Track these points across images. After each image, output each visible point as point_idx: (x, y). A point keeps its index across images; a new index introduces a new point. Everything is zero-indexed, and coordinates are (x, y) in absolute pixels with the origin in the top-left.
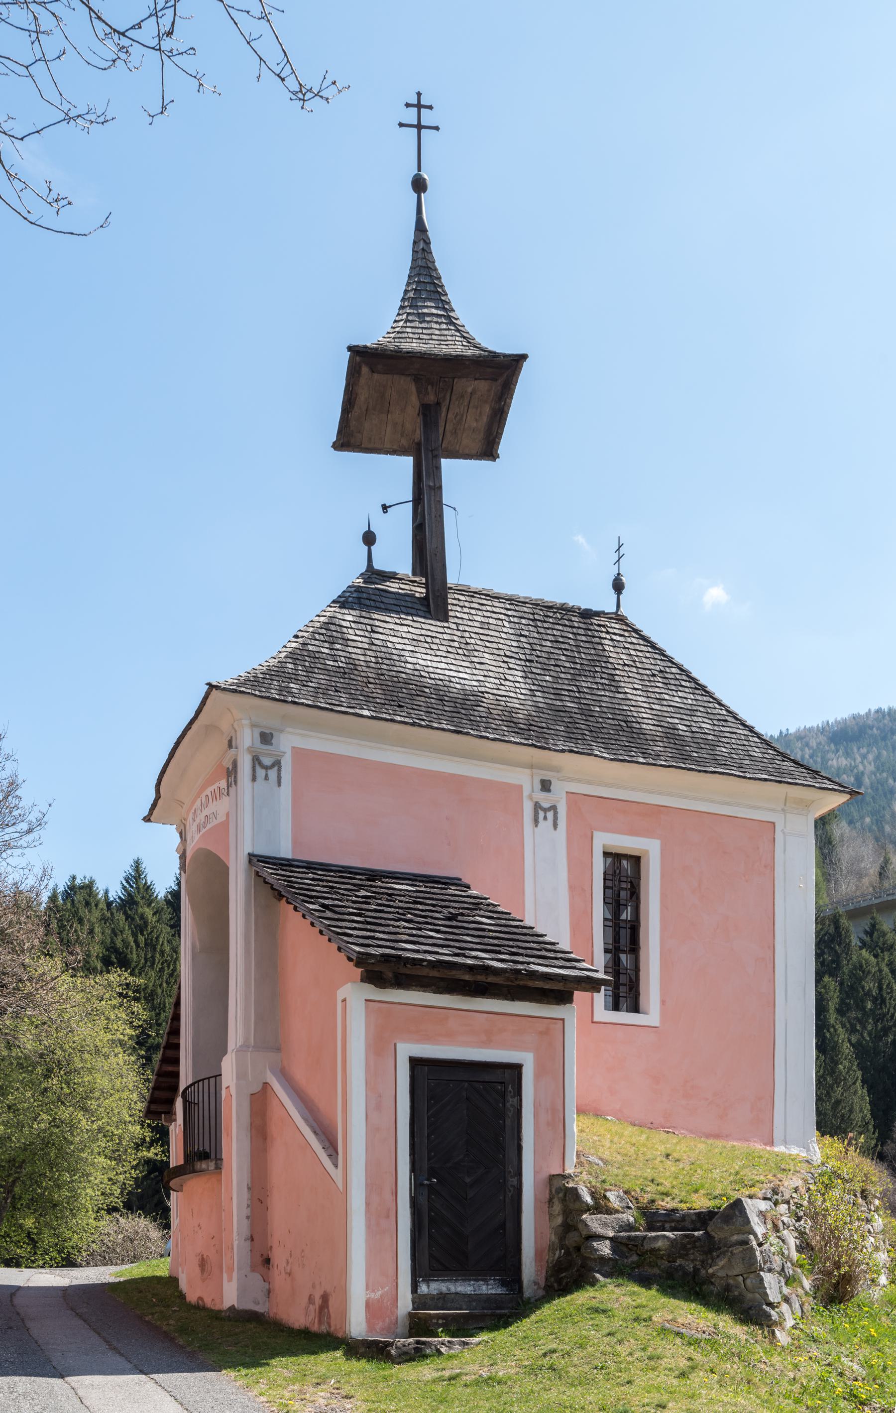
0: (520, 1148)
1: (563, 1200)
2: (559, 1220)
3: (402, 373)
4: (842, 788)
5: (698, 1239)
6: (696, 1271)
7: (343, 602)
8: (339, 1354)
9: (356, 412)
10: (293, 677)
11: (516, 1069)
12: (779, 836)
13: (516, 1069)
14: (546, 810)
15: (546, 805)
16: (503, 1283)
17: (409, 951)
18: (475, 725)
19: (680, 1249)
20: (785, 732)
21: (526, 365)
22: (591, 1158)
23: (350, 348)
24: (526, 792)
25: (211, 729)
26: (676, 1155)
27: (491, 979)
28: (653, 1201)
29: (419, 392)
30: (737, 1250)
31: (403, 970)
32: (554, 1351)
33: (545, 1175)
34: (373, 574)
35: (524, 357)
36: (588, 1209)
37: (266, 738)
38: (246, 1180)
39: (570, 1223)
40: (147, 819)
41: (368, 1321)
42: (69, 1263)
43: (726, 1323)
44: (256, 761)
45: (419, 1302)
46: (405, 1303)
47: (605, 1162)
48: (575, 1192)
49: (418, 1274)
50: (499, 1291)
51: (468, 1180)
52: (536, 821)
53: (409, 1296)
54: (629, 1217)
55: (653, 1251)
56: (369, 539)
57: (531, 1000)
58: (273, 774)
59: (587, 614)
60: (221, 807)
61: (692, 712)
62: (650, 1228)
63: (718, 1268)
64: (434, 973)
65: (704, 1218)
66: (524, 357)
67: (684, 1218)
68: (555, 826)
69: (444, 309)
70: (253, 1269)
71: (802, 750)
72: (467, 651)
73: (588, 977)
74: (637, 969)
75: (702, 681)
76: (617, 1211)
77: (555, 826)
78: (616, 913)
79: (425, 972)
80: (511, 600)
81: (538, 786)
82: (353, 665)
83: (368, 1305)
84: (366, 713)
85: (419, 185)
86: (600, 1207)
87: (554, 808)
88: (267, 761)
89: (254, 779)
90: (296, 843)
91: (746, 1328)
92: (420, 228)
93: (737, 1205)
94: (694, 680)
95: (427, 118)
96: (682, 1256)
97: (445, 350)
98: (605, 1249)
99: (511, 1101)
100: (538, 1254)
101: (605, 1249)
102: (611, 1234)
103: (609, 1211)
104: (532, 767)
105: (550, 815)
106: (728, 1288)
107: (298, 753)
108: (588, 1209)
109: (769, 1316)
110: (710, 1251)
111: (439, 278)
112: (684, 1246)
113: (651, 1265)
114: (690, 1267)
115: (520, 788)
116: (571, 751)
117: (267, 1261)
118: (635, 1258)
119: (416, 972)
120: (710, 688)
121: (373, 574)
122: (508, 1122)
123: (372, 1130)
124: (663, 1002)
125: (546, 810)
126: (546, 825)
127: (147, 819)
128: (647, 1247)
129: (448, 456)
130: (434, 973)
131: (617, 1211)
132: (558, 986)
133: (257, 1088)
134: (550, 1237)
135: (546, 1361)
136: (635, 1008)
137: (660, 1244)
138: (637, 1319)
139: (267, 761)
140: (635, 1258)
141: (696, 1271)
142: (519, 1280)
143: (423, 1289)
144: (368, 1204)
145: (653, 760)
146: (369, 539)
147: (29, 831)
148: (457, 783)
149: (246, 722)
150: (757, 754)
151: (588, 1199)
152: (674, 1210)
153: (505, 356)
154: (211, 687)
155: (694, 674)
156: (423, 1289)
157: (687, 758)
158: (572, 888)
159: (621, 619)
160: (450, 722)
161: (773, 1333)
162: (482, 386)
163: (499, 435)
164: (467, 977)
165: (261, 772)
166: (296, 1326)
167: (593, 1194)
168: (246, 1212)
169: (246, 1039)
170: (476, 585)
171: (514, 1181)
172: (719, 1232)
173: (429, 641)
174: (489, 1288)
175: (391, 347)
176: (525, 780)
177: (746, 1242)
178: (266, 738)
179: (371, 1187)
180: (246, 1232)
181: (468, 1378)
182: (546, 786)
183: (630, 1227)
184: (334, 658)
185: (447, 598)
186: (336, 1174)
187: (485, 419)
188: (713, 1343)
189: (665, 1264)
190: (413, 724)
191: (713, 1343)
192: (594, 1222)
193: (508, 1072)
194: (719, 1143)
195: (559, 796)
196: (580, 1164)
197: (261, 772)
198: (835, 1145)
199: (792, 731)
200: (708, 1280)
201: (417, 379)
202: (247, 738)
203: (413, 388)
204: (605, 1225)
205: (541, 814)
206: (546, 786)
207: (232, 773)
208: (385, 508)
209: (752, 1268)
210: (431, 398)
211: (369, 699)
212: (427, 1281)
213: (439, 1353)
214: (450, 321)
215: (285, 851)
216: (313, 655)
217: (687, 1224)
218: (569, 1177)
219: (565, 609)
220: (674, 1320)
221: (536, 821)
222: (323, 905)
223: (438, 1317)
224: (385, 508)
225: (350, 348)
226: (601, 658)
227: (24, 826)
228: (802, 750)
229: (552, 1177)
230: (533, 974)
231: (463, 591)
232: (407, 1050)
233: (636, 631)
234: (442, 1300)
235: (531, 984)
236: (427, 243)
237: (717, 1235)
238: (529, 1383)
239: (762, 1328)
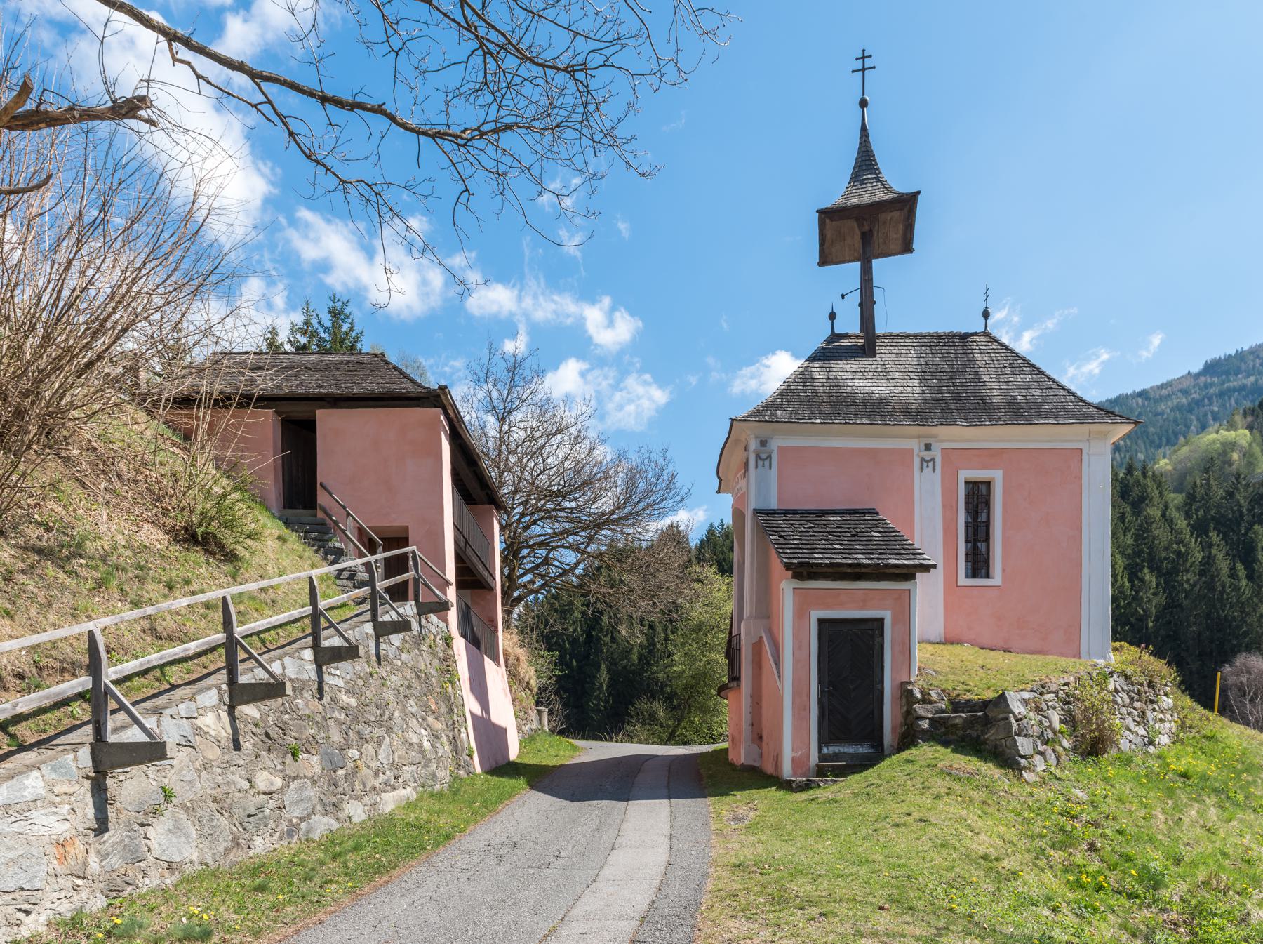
0: (882, 667)
1: (907, 697)
2: (905, 709)
3: (848, 218)
4: (1129, 420)
5: (979, 717)
6: (978, 737)
7: (812, 359)
8: (774, 788)
9: (827, 244)
10: (781, 407)
11: (880, 621)
12: (1085, 457)
13: (880, 621)
14: (927, 462)
15: (928, 459)
16: (872, 747)
17: (818, 558)
18: (883, 417)
19: (969, 723)
20: (1240, 350)
21: (920, 197)
22: (928, 671)
23: (818, 211)
24: (915, 453)
25: (737, 441)
26: (988, 666)
27: (863, 570)
28: (958, 695)
29: (859, 226)
30: (1002, 723)
31: (812, 570)
32: (872, 784)
33: (898, 682)
34: (835, 337)
35: (919, 193)
36: (918, 701)
37: (763, 443)
38: (750, 692)
39: (642, 705)
40: (718, 492)
41: (793, 769)
42: (715, 741)
43: (990, 770)
44: (758, 457)
45: (823, 758)
46: (814, 758)
47: (936, 672)
48: (911, 692)
49: (822, 742)
50: (870, 751)
51: (851, 687)
52: (922, 469)
53: (817, 754)
54: (943, 705)
55: (954, 725)
56: (832, 316)
57: (895, 580)
58: (767, 463)
59: (964, 337)
60: (743, 484)
61: (1028, 386)
62: (955, 711)
63: (991, 735)
64: (831, 570)
65: (986, 704)
66: (919, 193)
67: (975, 705)
68: (934, 470)
69: (876, 174)
70: (753, 741)
71: (1253, 361)
72: (886, 373)
73: (921, 564)
74: (988, 552)
75: (1038, 365)
76: (935, 702)
77: (934, 470)
78: (975, 519)
79: (825, 570)
80: (916, 336)
81: (923, 447)
82: (815, 391)
83: (793, 760)
84: (818, 421)
85: (863, 103)
86: (926, 699)
87: (933, 460)
88: (764, 456)
89: (757, 467)
90: (779, 500)
91: (1003, 771)
92: (864, 129)
93: (1002, 697)
94: (1033, 366)
95: (868, 63)
96: (970, 728)
97: (874, 199)
98: (925, 725)
99: (878, 640)
100: (894, 729)
101: (925, 725)
102: (930, 716)
103: (931, 702)
104: (919, 437)
105: (931, 464)
106: (996, 747)
107: (781, 449)
108: (918, 701)
109: (1019, 763)
110: (986, 725)
111: (874, 156)
112: (971, 722)
113: (952, 734)
114: (974, 734)
115: (912, 450)
116: (942, 424)
117: (761, 737)
118: (943, 730)
119: (819, 570)
120: (1043, 369)
121: (835, 337)
122: (875, 652)
123: (796, 662)
124: (1004, 570)
125: (927, 462)
126: (928, 471)
127: (718, 492)
128: (950, 722)
129: (877, 257)
130: (831, 570)
131: (935, 702)
132: (905, 571)
133: (755, 640)
134: (900, 719)
135: (866, 790)
136: (988, 576)
137: (957, 721)
138: (928, 766)
139: (764, 456)
140: (943, 730)
141: (978, 737)
142: (882, 744)
143: (825, 750)
144: (793, 703)
145: (995, 421)
146: (832, 316)
147: (681, 501)
148: (873, 454)
149: (752, 436)
150: (1070, 406)
151: (919, 696)
152: (969, 700)
153: (907, 194)
154: (733, 420)
155: (1033, 362)
156: (825, 750)
157: (1021, 416)
158: (944, 506)
159: (986, 334)
160: (868, 418)
161: (1021, 774)
162: (896, 214)
163: (912, 238)
164: (849, 571)
165: (760, 463)
166: (769, 773)
167: (922, 693)
168: (750, 710)
169: (751, 613)
170: (895, 331)
171: (879, 686)
172: (991, 713)
173: (863, 372)
174: (864, 750)
175: (842, 204)
176: (915, 445)
177: (1007, 718)
178: (763, 443)
179: (796, 693)
180: (749, 722)
181: (820, 800)
182: (928, 447)
183: (943, 711)
184: (805, 391)
185: (875, 346)
186: (780, 686)
187: (901, 232)
188: (970, 778)
189: (960, 733)
190: (845, 423)
191: (970, 778)
192: (920, 709)
193: (876, 623)
194: (1040, 657)
195: (936, 453)
196: (921, 674)
197: (760, 463)
198: (1131, 652)
199: (1246, 348)
200: (985, 742)
201: (857, 219)
202: (753, 445)
203: (856, 225)
204: (927, 710)
205: (925, 464)
206: (928, 447)
207: (746, 464)
208: (843, 296)
209: (1009, 734)
210: (866, 228)
211: (821, 412)
212: (827, 746)
213: (819, 786)
214: (878, 180)
215: (774, 504)
216: (793, 391)
217: (977, 708)
218: (911, 683)
219: (951, 336)
220: (951, 766)
221: (922, 469)
222: (781, 536)
223: (828, 766)
224: (843, 296)
225: (818, 211)
226: (972, 361)
227: (679, 498)
228: (1253, 361)
229: (902, 683)
230: (887, 566)
231: (886, 336)
232: (816, 614)
233: (996, 341)
234: (836, 757)
235: (887, 571)
236: (867, 136)
237: (990, 715)
238: (853, 802)
239: (1013, 770)
